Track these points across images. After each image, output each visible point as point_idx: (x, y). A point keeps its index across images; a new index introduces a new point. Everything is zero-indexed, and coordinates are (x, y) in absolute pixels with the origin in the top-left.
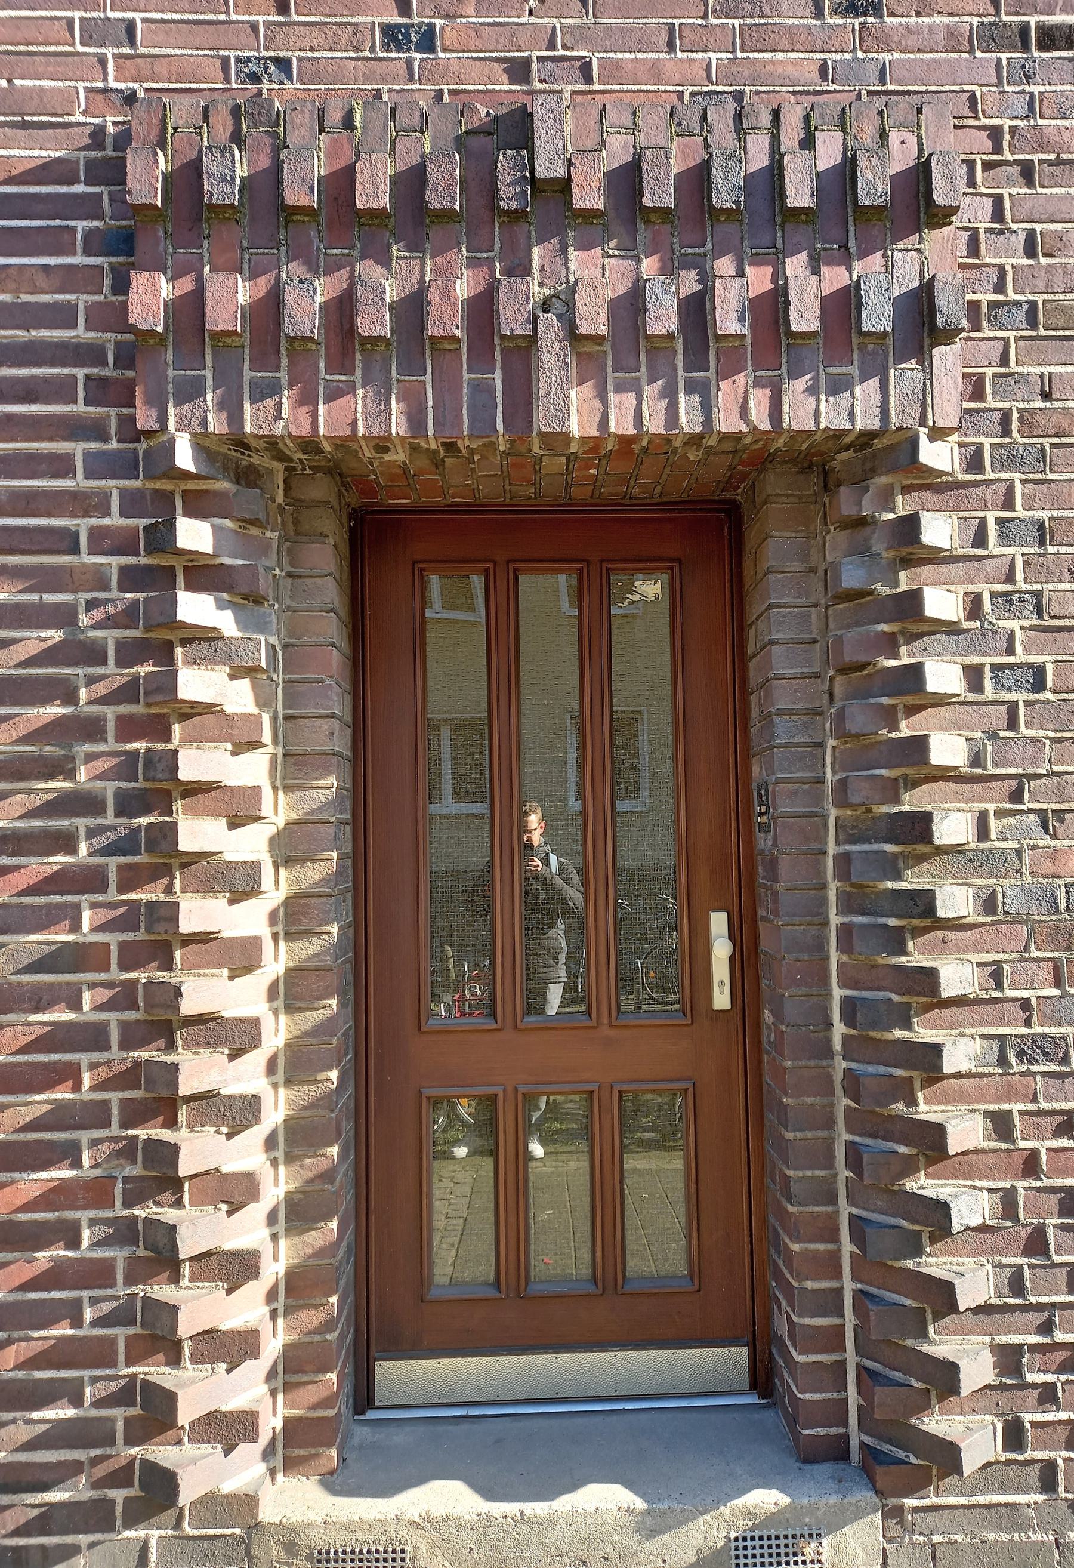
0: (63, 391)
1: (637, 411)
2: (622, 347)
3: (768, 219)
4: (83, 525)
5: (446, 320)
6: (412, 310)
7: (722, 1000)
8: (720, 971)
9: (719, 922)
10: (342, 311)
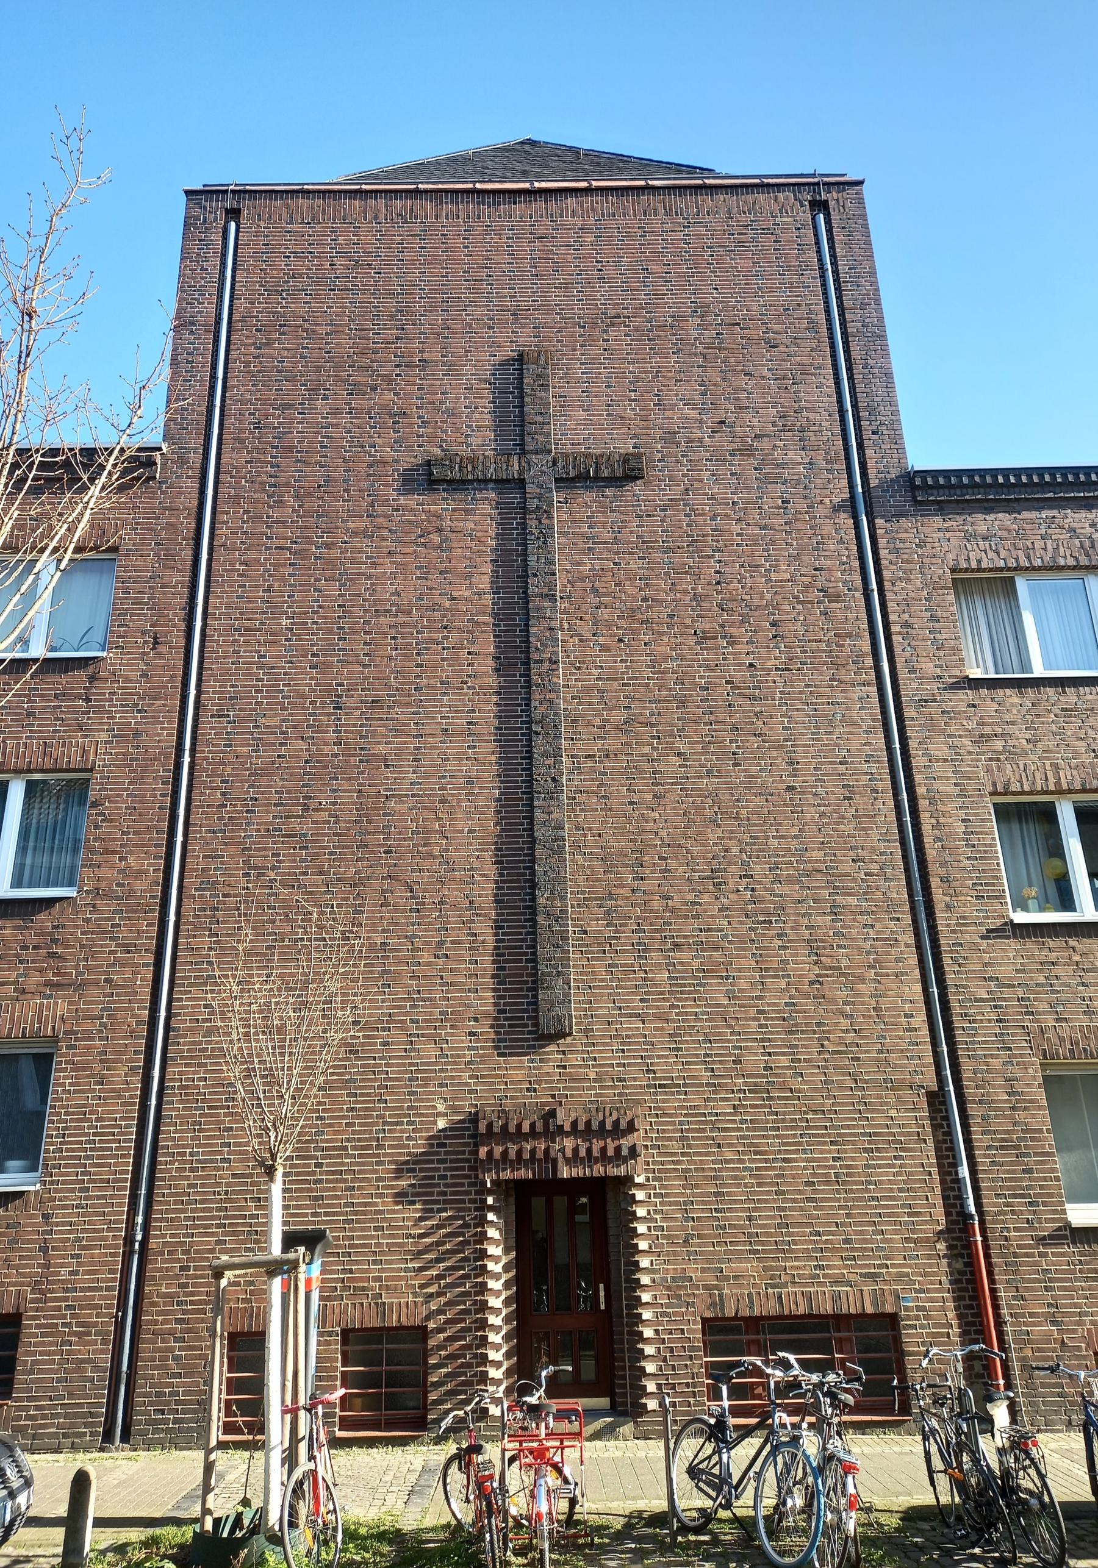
0: (463, 1169)
1: (577, 1172)
2: (574, 1159)
3: (602, 1132)
4: (466, 1198)
5: (540, 1155)
6: (533, 1151)
7: (603, 1307)
8: (602, 1300)
9: (601, 1286)
10: (519, 1153)
